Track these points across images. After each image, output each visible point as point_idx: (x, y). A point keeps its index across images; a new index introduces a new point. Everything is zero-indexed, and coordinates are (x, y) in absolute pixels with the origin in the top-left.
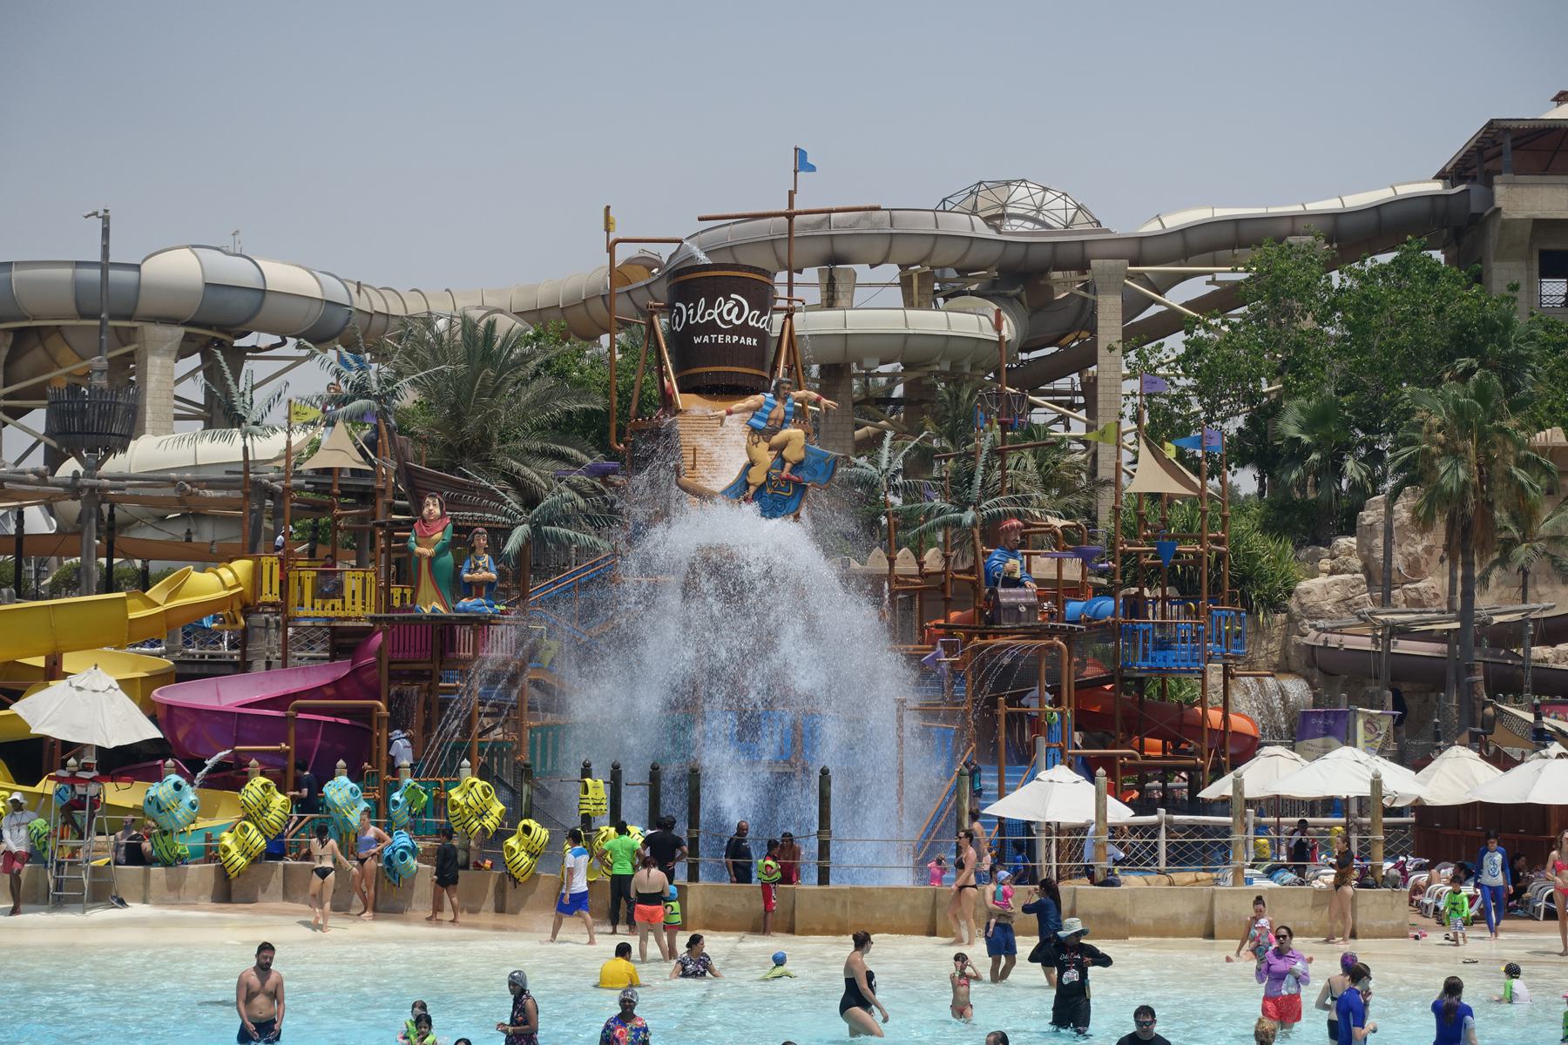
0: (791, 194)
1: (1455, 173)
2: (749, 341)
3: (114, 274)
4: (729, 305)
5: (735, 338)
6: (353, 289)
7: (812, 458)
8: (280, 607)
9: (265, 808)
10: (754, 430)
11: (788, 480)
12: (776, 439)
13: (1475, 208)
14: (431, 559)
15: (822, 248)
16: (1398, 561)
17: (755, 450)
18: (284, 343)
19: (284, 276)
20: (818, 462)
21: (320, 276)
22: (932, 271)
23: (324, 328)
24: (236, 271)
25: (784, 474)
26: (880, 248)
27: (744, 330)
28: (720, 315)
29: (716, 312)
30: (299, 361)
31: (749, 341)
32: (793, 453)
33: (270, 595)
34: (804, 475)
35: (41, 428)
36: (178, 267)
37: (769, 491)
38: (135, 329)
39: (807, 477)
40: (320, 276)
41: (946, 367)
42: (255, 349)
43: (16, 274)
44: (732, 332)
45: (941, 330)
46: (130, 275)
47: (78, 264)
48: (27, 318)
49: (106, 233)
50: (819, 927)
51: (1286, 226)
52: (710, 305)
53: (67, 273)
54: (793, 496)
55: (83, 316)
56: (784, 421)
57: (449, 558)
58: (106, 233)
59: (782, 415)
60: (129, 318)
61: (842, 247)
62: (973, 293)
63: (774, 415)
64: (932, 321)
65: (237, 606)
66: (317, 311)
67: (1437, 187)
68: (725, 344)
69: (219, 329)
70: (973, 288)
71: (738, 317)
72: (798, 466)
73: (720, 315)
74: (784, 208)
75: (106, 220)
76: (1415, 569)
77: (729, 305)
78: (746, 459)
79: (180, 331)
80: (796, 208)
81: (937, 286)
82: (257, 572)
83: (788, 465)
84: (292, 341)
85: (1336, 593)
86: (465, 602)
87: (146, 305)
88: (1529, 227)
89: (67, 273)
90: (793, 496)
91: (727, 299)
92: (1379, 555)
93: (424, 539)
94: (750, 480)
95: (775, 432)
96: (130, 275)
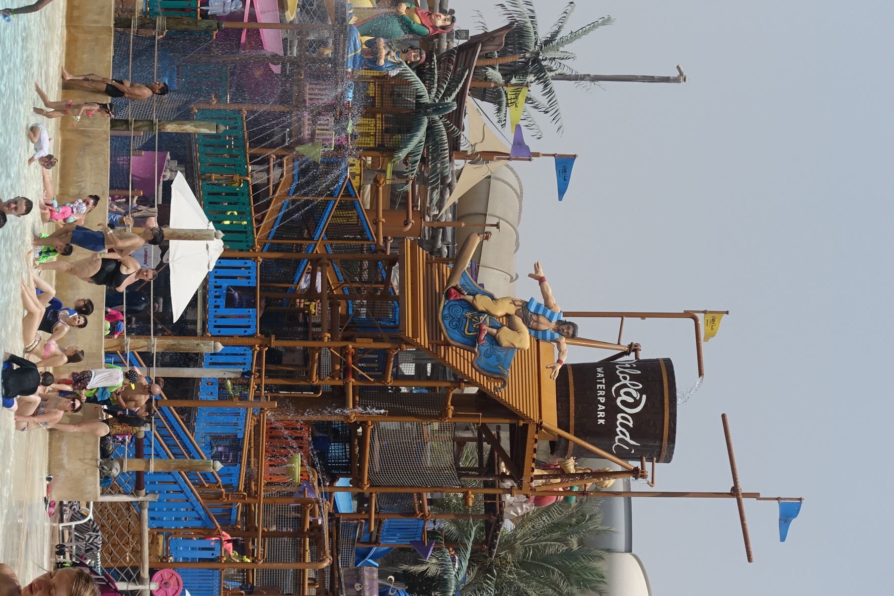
0: (756, 496)
2: (601, 414)
3: (620, 502)
4: (634, 394)
5: (602, 400)
7: (502, 354)
10: (526, 305)
11: (480, 330)
12: (519, 321)
17: (507, 302)
20: (498, 358)
25: (485, 327)
27: (612, 410)
28: (625, 386)
29: (627, 382)
31: (601, 414)
32: (506, 336)
34: (484, 345)
37: (469, 314)
39: (483, 349)
44: (608, 395)
49: (666, 80)
52: (633, 377)
54: (464, 336)
56: (536, 330)
58: (666, 80)
59: (543, 327)
63: (542, 319)
68: (596, 391)
71: (624, 403)
72: (494, 340)
73: (625, 386)
74: (743, 488)
75: (676, 80)
76: (522, 509)
77: (634, 394)
78: (497, 296)
80: (744, 501)
83: (495, 331)
90: (464, 336)
91: (641, 392)
94: (478, 296)
95: (526, 321)
96: (620, 541)
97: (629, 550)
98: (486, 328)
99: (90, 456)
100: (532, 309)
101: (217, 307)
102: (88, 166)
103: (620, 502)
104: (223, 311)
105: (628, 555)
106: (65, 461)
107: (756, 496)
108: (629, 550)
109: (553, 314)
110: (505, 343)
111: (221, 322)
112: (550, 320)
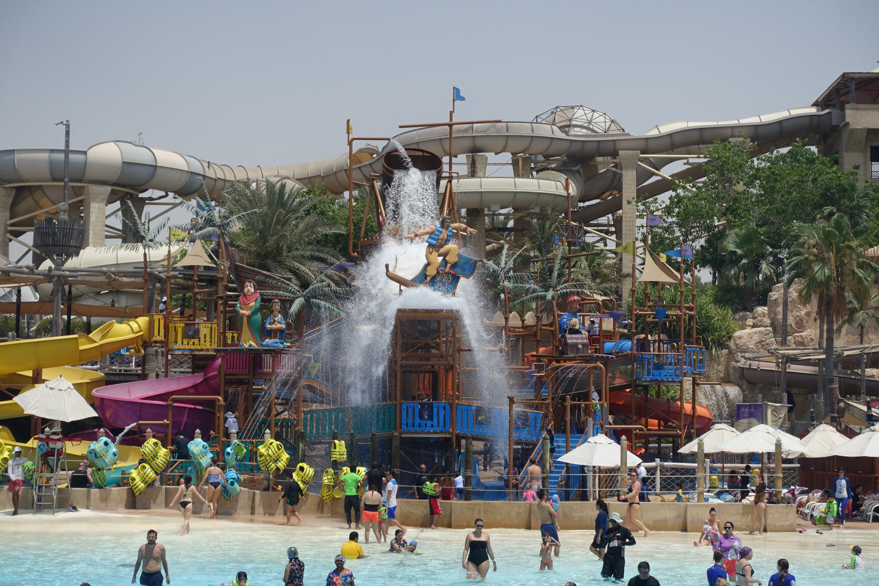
0: (451, 113)
1: (824, 103)
3: (72, 156)
6: (206, 165)
7: (462, 261)
8: (164, 343)
9: (155, 456)
12: (442, 250)
13: (834, 123)
14: (249, 317)
15: (468, 144)
16: (791, 320)
18: (167, 195)
19: (167, 158)
20: (465, 263)
21: (188, 158)
22: (529, 157)
23: (188, 187)
24: (140, 155)
26: (501, 143)
30: (175, 205)
32: (452, 258)
33: (159, 337)
35: (30, 242)
36: (107, 153)
38: (83, 187)
40: (188, 158)
41: (537, 210)
42: (151, 199)
43: (17, 156)
45: (535, 189)
46: (81, 157)
47: (52, 151)
48: (23, 181)
49: (67, 133)
50: (465, 524)
51: (729, 132)
53: (46, 156)
55: (54, 180)
57: (258, 316)
58: (67, 133)
59: (446, 236)
60: (80, 181)
61: (479, 143)
62: (553, 169)
63: (441, 237)
64: (530, 185)
65: (140, 343)
66: (185, 178)
67: (813, 110)
69: (130, 188)
70: (553, 166)
72: (454, 265)
74: (447, 121)
75: (68, 126)
79: (109, 189)
80: (454, 121)
81: (532, 165)
82: (151, 324)
83: (449, 265)
84: (171, 195)
85: (756, 338)
86: (268, 341)
87: (89, 175)
88: (865, 134)
89: (46, 156)
92: (780, 317)
93: (245, 305)
95: (442, 246)
96: (81, 157)
97: (85, 153)
98: (447, 270)
99: (785, 510)
100: (434, 242)
101: (432, 426)
102: (580, 514)
103: (71, 156)
104: (435, 422)
105: (88, 153)
106: (788, 523)
107: (451, 113)
108: (85, 153)
109: (437, 230)
110: (456, 259)
111: (441, 423)
112: (441, 232)
